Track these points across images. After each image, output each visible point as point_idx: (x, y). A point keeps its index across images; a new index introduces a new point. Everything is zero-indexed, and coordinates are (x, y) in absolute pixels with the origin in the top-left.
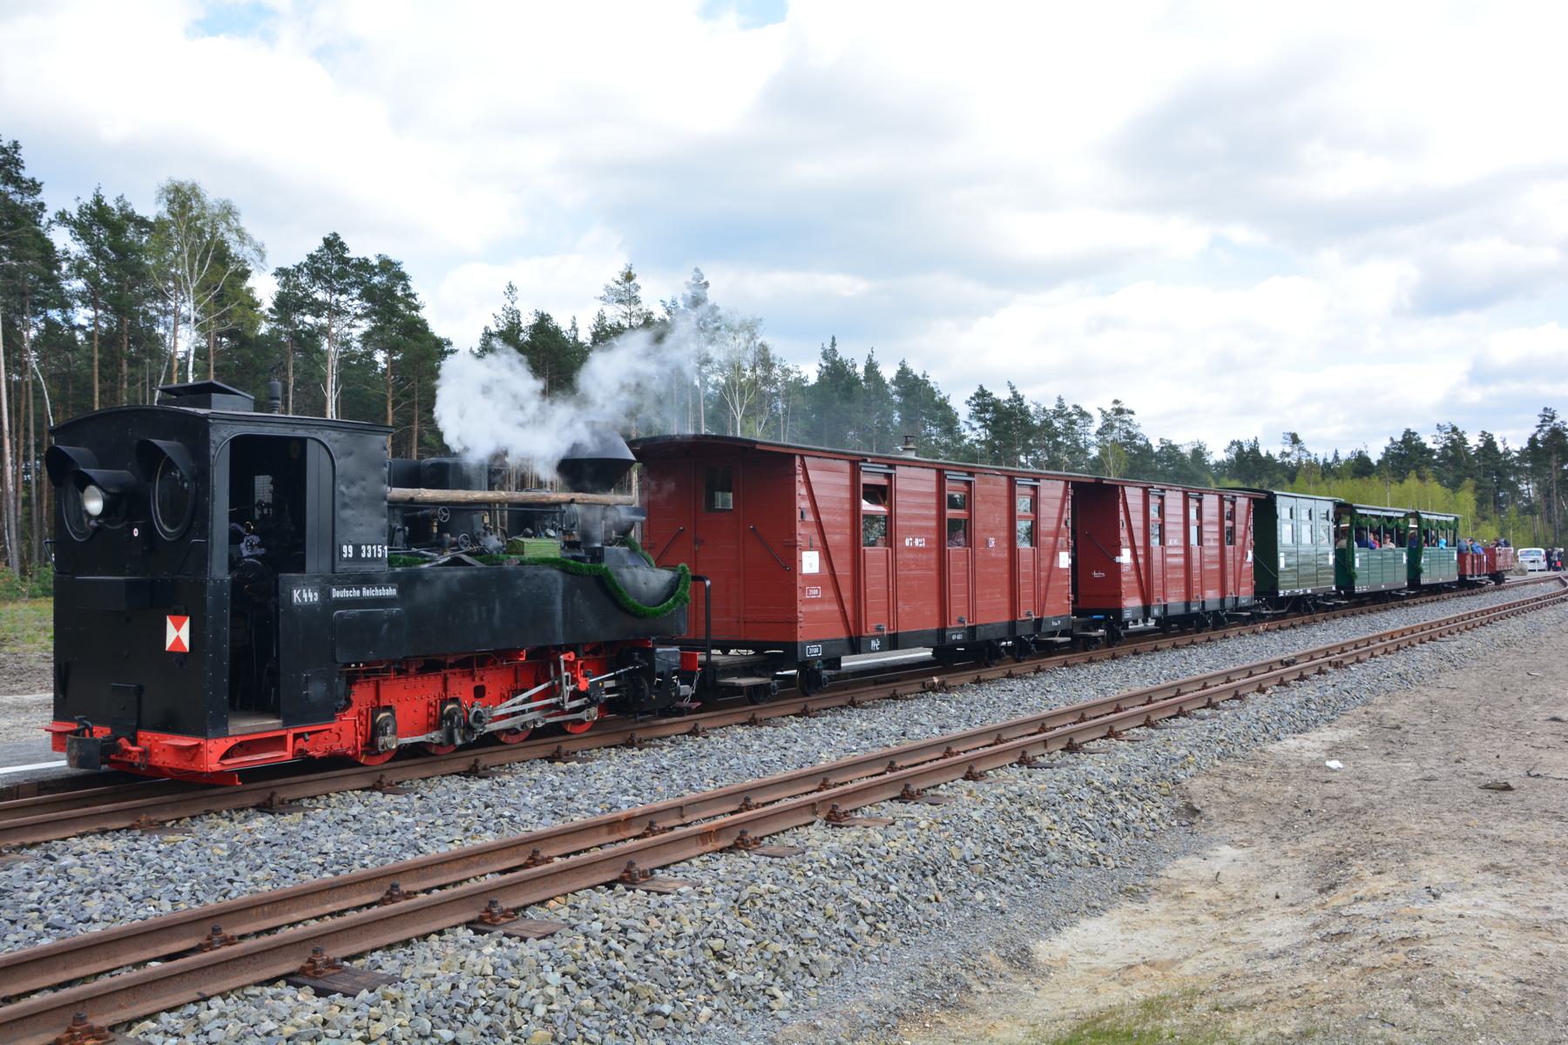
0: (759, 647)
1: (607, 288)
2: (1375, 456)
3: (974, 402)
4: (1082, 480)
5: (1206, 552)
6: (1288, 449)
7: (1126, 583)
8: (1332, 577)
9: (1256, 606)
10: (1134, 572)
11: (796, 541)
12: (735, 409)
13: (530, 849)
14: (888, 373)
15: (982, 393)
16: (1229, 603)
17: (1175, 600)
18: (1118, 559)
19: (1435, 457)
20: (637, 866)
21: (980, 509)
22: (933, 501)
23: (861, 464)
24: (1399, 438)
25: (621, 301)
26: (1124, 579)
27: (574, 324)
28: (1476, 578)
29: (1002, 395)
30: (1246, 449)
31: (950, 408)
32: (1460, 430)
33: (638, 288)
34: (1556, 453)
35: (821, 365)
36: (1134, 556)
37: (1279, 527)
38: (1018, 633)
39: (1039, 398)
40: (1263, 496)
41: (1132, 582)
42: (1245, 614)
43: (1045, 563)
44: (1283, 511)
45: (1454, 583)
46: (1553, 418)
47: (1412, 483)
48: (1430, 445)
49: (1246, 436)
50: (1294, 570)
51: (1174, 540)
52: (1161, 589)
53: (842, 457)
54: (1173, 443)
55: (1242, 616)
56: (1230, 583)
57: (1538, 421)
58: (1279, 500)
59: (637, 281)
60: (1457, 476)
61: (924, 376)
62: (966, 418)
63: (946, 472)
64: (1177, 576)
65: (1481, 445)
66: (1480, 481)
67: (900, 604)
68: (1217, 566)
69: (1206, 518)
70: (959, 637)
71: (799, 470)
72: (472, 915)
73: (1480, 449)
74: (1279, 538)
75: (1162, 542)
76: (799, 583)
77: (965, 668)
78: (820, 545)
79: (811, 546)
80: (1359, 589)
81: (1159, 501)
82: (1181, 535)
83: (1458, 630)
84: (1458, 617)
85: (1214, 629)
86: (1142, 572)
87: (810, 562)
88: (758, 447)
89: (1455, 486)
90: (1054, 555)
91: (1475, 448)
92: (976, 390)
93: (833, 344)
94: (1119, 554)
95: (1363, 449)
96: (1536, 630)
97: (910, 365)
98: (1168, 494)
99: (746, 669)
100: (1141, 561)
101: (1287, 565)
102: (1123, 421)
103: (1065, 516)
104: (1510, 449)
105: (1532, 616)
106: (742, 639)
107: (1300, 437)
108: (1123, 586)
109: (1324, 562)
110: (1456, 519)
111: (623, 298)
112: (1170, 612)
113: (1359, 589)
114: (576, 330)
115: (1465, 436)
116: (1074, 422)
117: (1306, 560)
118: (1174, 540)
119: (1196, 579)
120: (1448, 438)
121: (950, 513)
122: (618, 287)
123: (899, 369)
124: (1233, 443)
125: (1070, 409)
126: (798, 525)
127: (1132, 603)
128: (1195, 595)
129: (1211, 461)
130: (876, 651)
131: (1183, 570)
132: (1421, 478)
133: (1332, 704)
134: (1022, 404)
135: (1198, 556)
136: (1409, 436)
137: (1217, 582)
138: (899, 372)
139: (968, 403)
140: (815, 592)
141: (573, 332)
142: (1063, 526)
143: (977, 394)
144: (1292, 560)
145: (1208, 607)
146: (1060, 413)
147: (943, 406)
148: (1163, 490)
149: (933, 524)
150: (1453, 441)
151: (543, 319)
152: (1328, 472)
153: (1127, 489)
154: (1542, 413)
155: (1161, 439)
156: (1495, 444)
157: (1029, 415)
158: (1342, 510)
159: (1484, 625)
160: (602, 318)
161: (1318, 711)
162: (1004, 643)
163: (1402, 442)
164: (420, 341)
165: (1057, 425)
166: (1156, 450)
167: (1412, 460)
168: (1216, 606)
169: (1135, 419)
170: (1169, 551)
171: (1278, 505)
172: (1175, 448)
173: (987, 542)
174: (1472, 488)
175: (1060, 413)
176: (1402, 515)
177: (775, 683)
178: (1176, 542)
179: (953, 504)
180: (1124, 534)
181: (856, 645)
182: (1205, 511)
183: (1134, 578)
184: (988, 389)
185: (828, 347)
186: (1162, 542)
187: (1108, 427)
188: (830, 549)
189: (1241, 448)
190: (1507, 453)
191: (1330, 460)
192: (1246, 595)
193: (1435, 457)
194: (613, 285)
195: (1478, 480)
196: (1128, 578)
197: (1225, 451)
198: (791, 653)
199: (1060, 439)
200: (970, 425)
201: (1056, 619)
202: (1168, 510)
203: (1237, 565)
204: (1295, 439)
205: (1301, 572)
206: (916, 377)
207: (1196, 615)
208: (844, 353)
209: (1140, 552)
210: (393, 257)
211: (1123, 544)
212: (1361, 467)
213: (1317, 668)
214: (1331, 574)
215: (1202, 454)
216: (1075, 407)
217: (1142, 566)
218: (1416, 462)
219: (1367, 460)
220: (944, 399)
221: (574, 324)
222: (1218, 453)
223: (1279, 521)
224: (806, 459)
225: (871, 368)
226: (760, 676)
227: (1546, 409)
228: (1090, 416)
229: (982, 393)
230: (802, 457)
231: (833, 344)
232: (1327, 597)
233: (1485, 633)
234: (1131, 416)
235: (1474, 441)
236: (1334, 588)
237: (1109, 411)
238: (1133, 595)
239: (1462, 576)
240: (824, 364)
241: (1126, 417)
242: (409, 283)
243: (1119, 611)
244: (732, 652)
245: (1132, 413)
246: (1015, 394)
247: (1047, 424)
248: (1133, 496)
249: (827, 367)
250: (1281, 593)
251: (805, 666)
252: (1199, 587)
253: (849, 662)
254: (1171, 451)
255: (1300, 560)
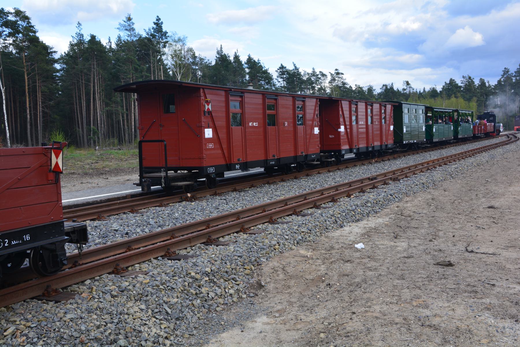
0: (189, 169)
1: (120, 24)
2: (439, 89)
3: (279, 71)
4: (323, 98)
5: (375, 126)
6: (405, 88)
7: (343, 139)
8: (424, 136)
9: (394, 148)
10: (346, 135)
11: (202, 124)
12: (178, 75)
13: (439, 164)
14: (243, 59)
15: (282, 67)
16: (384, 147)
17: (362, 145)
18: (339, 130)
19: (462, 89)
20: (120, 266)
21: (281, 110)
22: (261, 107)
23: (229, 92)
24: (448, 82)
25: (126, 30)
26: (342, 138)
27: (110, 40)
28: (479, 135)
29: (290, 67)
30: (389, 87)
31: (269, 73)
32: (472, 78)
33: (133, 24)
34: (509, 86)
35: (216, 57)
36: (346, 128)
37: (403, 116)
38: (298, 161)
39: (305, 69)
40: (397, 104)
41: (345, 139)
42: (390, 151)
43: (309, 132)
44: (405, 111)
45: (472, 137)
46: (508, 72)
47: (453, 99)
48: (460, 84)
49: (388, 82)
50: (409, 133)
51: (362, 122)
52: (357, 142)
53: (221, 89)
54: (360, 86)
55: (389, 152)
56: (384, 139)
57: (502, 73)
58: (404, 105)
59: (133, 21)
60: (470, 96)
61: (258, 60)
62: (276, 78)
63: (266, 95)
64: (363, 136)
65: (480, 84)
66: (479, 98)
67: (248, 150)
68: (379, 132)
69: (374, 113)
70: (273, 163)
71: (202, 94)
72: (204, 240)
73: (479, 85)
74: (403, 121)
75: (357, 122)
76: (204, 142)
77: (278, 175)
78: (212, 126)
79: (209, 127)
80: (435, 140)
81: (356, 106)
82: (365, 120)
83: (458, 159)
84: (461, 153)
85: (378, 157)
86: (349, 135)
87: (208, 133)
88: (183, 84)
89: (469, 100)
90: (312, 129)
91: (477, 85)
92: (280, 66)
93: (221, 48)
94: (340, 128)
95: (435, 87)
96: (493, 158)
97: (252, 56)
98: (359, 103)
99: (183, 178)
100: (348, 130)
101: (406, 131)
102: (339, 78)
103: (316, 113)
104: (491, 85)
105: (492, 152)
106: (181, 166)
107: (410, 83)
108: (342, 141)
109: (421, 130)
110: (472, 112)
111: (128, 28)
112: (361, 151)
113: (435, 140)
114: (111, 43)
115: (474, 80)
116: (320, 78)
117: (414, 129)
118: (362, 122)
119: (370, 137)
120: (467, 81)
121: (268, 112)
122: (125, 23)
123: (248, 58)
124: (384, 85)
125: (318, 73)
126: (203, 118)
127: (346, 147)
128: (370, 144)
129: (375, 93)
130: (238, 169)
131: (365, 134)
132: (456, 97)
133: (381, 203)
134: (298, 71)
135: (371, 128)
136: (452, 81)
137: (379, 138)
138: (248, 59)
139: (277, 71)
140: (211, 146)
141: (109, 44)
142: (316, 117)
143: (280, 68)
144: (409, 129)
145: (376, 149)
146: (314, 74)
147: (266, 72)
148: (357, 102)
149: (261, 116)
150: (469, 82)
151: (93, 37)
152: (421, 96)
153: (343, 102)
154: (504, 70)
155: (356, 85)
156: (485, 83)
157: (301, 76)
158: (428, 109)
159: (471, 157)
160: (119, 37)
161: (372, 207)
162: (293, 165)
163: (449, 84)
164: (36, 46)
165: (313, 79)
166: (354, 89)
167: (453, 90)
168: (379, 148)
169: (344, 77)
170: (360, 127)
171: (403, 108)
172: (361, 88)
173: (284, 124)
174: (476, 101)
175: (314, 74)
176: (451, 111)
177: (196, 184)
178: (362, 123)
179: (269, 109)
180: (341, 120)
181: (230, 167)
182: (374, 110)
183: (346, 137)
184: (284, 65)
185: (219, 49)
186: (357, 122)
187: (333, 80)
188: (217, 128)
189: (386, 87)
190: (489, 86)
191: (422, 91)
192: (390, 142)
193: (462, 89)
194: (123, 23)
195: (478, 97)
196: (343, 138)
197: (381, 89)
198: (202, 172)
199: (314, 85)
200: (278, 80)
201: (313, 155)
202: (359, 110)
203: (387, 132)
204: (408, 83)
205: (412, 133)
206: (254, 61)
207: (371, 152)
208: (225, 52)
209: (348, 127)
210: (22, 9)
211: (341, 124)
212: (433, 93)
213: (427, 168)
214: (423, 134)
215: (371, 90)
216: (320, 72)
217: (349, 133)
218: (455, 91)
219: (436, 91)
220: (267, 70)
221: (110, 40)
222: (377, 90)
223: (403, 114)
224: (206, 90)
225: (236, 57)
226: (189, 181)
227: (505, 68)
228: (326, 76)
229: (282, 67)
230: (203, 89)
231: (221, 48)
232: (422, 143)
233: (471, 160)
234: (343, 75)
235: (477, 82)
236: (425, 140)
237: (333, 73)
238: (346, 144)
239: (474, 135)
240: (218, 56)
241: (341, 76)
242: (30, 21)
243: (340, 151)
244: (179, 172)
245: (343, 74)
246: (296, 67)
247: (309, 79)
248: (345, 105)
249: (219, 57)
250: (404, 142)
251: (208, 176)
252: (372, 141)
253: (228, 174)
254: (360, 90)
255: (412, 129)
